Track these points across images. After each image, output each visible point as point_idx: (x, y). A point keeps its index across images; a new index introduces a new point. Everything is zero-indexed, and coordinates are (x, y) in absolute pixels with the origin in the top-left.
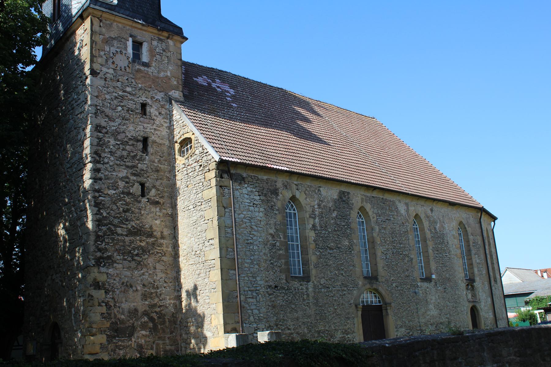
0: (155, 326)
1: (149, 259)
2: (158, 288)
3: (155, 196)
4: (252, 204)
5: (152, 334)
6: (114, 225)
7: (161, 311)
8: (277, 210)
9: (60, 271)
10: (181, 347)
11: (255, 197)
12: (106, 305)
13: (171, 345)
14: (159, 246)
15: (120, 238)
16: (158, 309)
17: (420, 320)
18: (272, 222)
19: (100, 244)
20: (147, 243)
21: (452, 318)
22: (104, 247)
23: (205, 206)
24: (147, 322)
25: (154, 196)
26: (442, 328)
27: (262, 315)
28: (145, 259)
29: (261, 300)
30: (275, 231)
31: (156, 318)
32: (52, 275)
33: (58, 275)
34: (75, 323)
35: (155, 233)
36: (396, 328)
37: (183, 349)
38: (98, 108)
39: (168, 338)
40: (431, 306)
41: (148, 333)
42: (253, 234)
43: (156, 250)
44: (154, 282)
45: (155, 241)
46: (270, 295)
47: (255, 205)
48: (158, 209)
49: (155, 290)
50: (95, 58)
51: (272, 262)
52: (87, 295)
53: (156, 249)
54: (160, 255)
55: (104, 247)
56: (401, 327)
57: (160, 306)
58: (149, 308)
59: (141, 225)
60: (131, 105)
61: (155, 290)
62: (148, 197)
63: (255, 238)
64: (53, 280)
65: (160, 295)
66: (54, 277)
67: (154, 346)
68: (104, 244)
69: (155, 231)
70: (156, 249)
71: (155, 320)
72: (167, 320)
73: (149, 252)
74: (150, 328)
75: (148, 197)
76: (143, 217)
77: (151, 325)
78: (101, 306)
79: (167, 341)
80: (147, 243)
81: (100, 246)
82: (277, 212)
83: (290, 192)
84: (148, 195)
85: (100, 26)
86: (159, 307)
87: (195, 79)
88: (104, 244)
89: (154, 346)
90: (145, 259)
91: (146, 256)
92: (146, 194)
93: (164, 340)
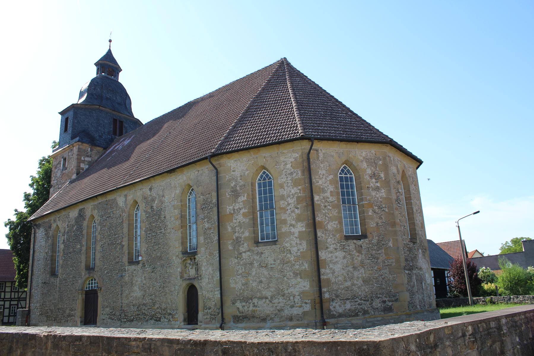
17: (123, 301)
21: (157, 299)
26: (144, 309)
36: (103, 308)
40: (136, 288)
56: (107, 307)
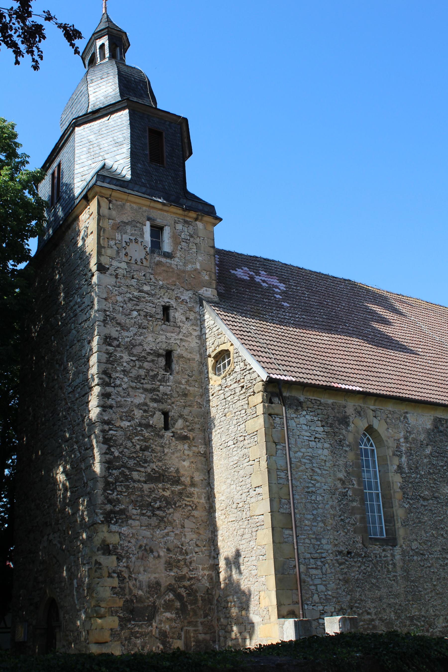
0: (184, 606)
1: (175, 514)
2: (187, 554)
3: (183, 429)
4: (312, 439)
5: (180, 617)
7: (192, 585)
8: (348, 446)
9: (59, 530)
12: (118, 577)
13: (205, 634)
14: (188, 497)
15: (136, 485)
16: (187, 583)
18: (341, 463)
19: (110, 494)
20: (173, 492)
24: (173, 601)
25: (181, 429)
27: (330, 593)
28: (170, 514)
29: (329, 571)
30: (345, 474)
31: (184, 594)
34: (78, 600)
35: (183, 479)
37: (222, 639)
39: (202, 623)
42: (315, 480)
43: (184, 502)
44: (182, 545)
45: (183, 489)
46: (340, 564)
47: (317, 440)
48: (186, 446)
49: (183, 557)
51: (342, 517)
53: (184, 500)
54: (190, 508)
57: (190, 579)
58: (176, 581)
59: (164, 468)
61: (183, 557)
62: (173, 430)
63: (318, 485)
67: (183, 634)
68: (115, 493)
69: (183, 475)
70: (184, 500)
72: (200, 598)
73: (175, 504)
74: (177, 609)
75: (173, 430)
77: (178, 604)
78: (112, 577)
79: (200, 628)
80: (173, 492)
81: (110, 497)
82: (347, 449)
84: (173, 427)
85: (110, 209)
86: (188, 580)
88: (115, 493)
89: (183, 634)
90: (170, 514)
91: (171, 510)
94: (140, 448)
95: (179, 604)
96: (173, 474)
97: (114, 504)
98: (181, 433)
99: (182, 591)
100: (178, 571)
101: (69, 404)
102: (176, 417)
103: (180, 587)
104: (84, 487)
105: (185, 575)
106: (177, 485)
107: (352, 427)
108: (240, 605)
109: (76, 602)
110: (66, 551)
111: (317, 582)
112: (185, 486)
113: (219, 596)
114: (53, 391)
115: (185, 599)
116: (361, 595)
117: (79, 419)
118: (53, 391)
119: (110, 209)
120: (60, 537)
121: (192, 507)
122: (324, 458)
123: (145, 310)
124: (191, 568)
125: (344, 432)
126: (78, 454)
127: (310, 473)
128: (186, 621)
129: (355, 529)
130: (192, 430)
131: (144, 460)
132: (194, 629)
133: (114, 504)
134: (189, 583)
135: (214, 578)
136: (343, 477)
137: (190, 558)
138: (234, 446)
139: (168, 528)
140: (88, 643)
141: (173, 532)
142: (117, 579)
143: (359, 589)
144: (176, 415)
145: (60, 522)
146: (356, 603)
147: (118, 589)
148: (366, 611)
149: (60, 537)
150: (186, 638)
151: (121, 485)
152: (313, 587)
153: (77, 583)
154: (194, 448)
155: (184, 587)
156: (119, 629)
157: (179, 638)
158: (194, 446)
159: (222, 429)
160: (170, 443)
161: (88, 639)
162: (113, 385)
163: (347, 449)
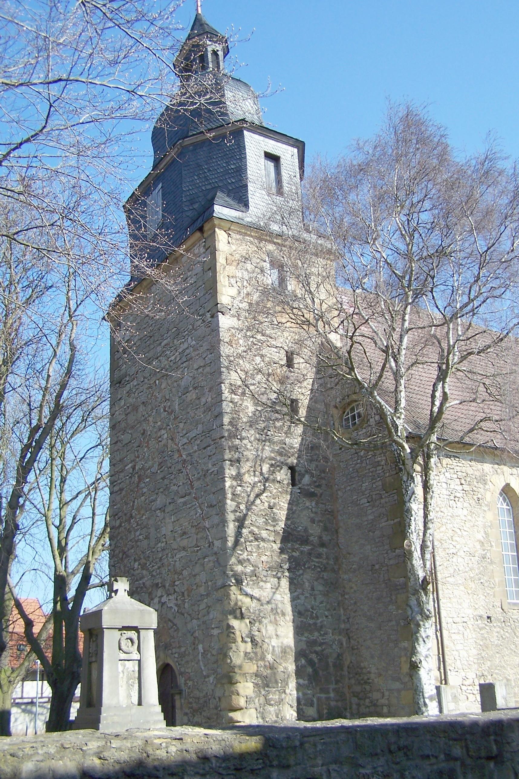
0: (315, 671)
1: (305, 576)
2: (317, 617)
3: (310, 485)
4: (452, 498)
5: (312, 683)
6: (258, 527)
7: (323, 650)
8: (486, 505)
9: (175, 591)
10: (351, 703)
11: (456, 487)
12: (252, 641)
13: (337, 701)
14: (317, 558)
15: (266, 545)
16: (318, 649)
18: (480, 523)
19: (241, 555)
20: (302, 552)
22: (246, 557)
23: (387, 500)
24: (305, 666)
25: (308, 485)
27: (471, 659)
28: (299, 576)
29: (470, 637)
30: (484, 536)
31: (316, 661)
32: (162, 596)
33: (170, 597)
34: (205, 666)
35: (311, 538)
37: (354, 706)
38: (232, 358)
39: (334, 690)
41: (306, 682)
42: (456, 541)
43: (313, 563)
44: (312, 608)
45: (312, 549)
46: (481, 629)
47: (456, 499)
48: (313, 504)
49: (313, 621)
50: (224, 289)
51: (482, 581)
52: (225, 627)
53: (313, 561)
54: (319, 570)
55: (246, 557)
57: (321, 644)
58: (308, 646)
59: (292, 526)
60: (273, 353)
61: (313, 621)
62: (300, 486)
63: (458, 547)
64: (163, 604)
65: (321, 627)
66: (164, 599)
67: (315, 700)
68: (246, 554)
69: (312, 535)
70: (313, 561)
71: (315, 663)
72: (331, 664)
73: (304, 565)
74: (309, 675)
75: (300, 486)
76: (295, 516)
77: (310, 670)
78: (246, 642)
79: (332, 695)
80: (302, 552)
81: (241, 557)
82: (486, 509)
83: (502, 479)
84: (300, 483)
85: (229, 243)
86: (320, 646)
87: (160, 186)
88: (246, 554)
89: (315, 700)
90: (299, 576)
91: (301, 572)
92: (297, 482)
93: (328, 693)
94: (269, 505)
95: (311, 670)
96: (301, 533)
97: (244, 565)
98: (308, 489)
99: (314, 656)
100: (310, 636)
101: (184, 456)
102: (303, 472)
103: (311, 652)
104: (209, 546)
105: (316, 640)
106: (306, 545)
107: (490, 486)
108: (376, 671)
109: (203, 668)
110: (185, 615)
111: (459, 647)
112: (314, 546)
113: (351, 662)
114: (160, 441)
115: (317, 665)
116: (500, 661)
117: (198, 473)
118: (160, 441)
119: (229, 243)
120: (177, 600)
121: (321, 568)
122: (464, 518)
123: (269, 355)
124: (322, 633)
125: (482, 490)
126: (199, 511)
127: (451, 533)
128: (318, 688)
129: (494, 592)
130: (319, 486)
131: (273, 518)
132: (325, 696)
133: (244, 565)
134: (320, 648)
135: (344, 644)
136: (482, 539)
137: (321, 622)
138: (368, 504)
139: (298, 590)
140: (220, 710)
141: (303, 594)
142: (250, 644)
143: (497, 655)
144: (303, 471)
145: (176, 583)
146: (496, 669)
147: (252, 654)
148: (506, 678)
149: (177, 600)
150: (318, 704)
151: (251, 545)
152: (455, 653)
153: (203, 648)
154: (321, 505)
155: (316, 652)
156: (253, 696)
157: (312, 705)
158: (322, 503)
159: (354, 486)
160: (298, 500)
161: (220, 706)
162: (239, 437)
163: (486, 509)
